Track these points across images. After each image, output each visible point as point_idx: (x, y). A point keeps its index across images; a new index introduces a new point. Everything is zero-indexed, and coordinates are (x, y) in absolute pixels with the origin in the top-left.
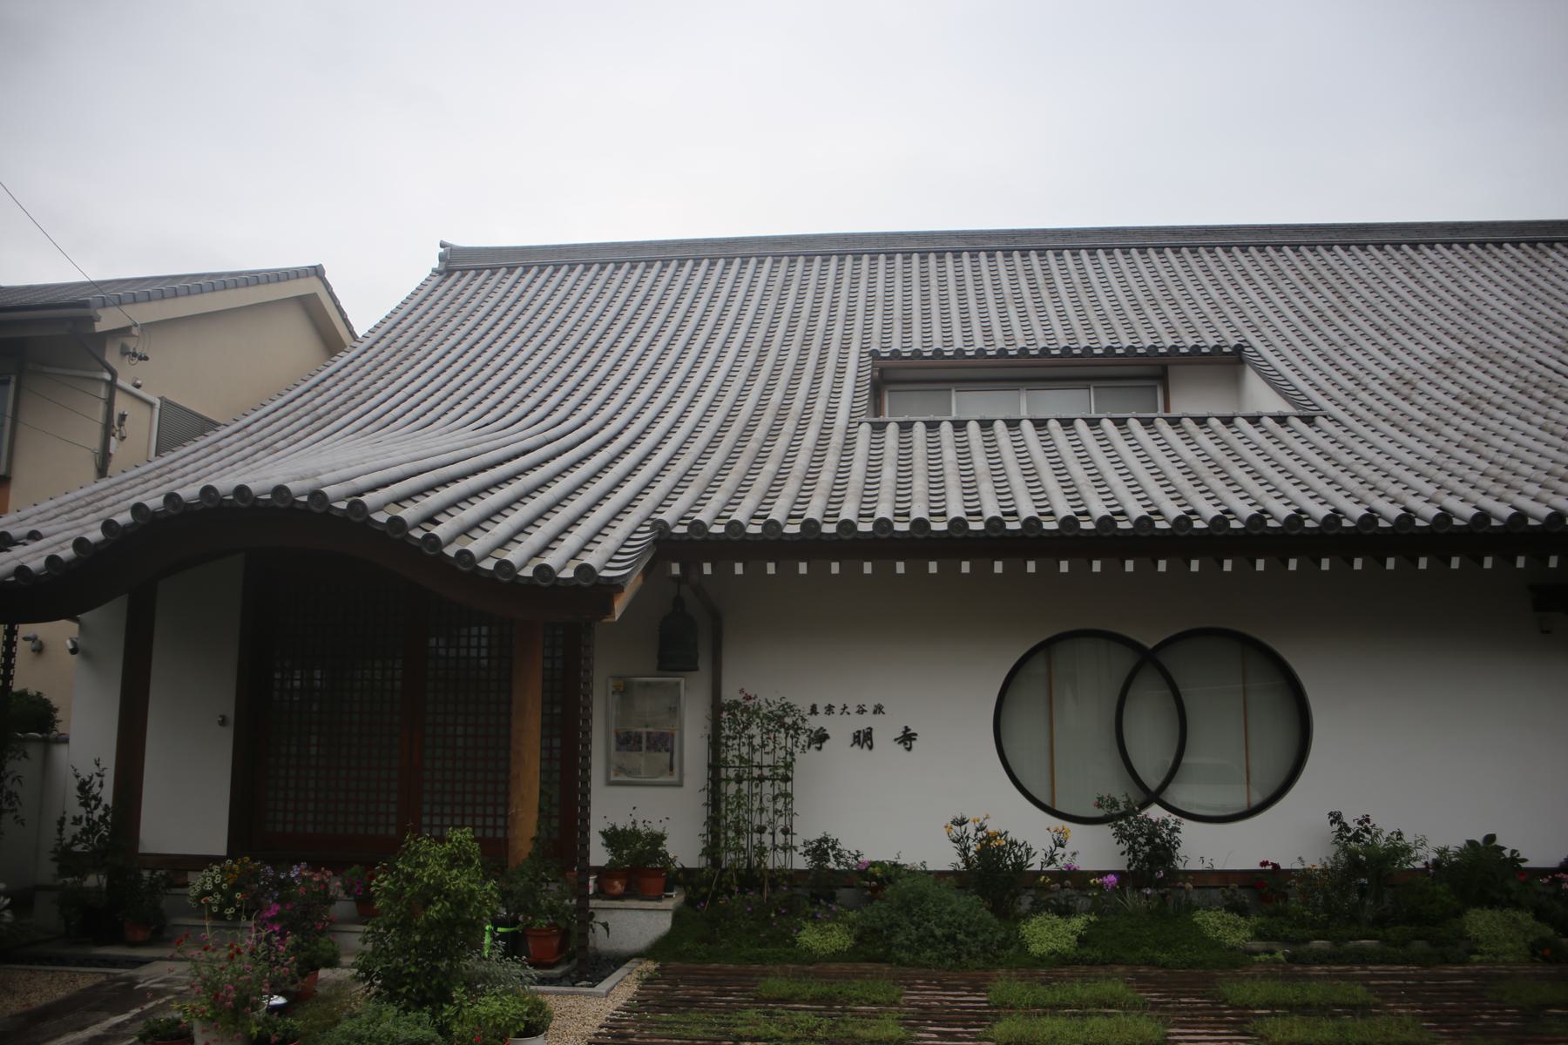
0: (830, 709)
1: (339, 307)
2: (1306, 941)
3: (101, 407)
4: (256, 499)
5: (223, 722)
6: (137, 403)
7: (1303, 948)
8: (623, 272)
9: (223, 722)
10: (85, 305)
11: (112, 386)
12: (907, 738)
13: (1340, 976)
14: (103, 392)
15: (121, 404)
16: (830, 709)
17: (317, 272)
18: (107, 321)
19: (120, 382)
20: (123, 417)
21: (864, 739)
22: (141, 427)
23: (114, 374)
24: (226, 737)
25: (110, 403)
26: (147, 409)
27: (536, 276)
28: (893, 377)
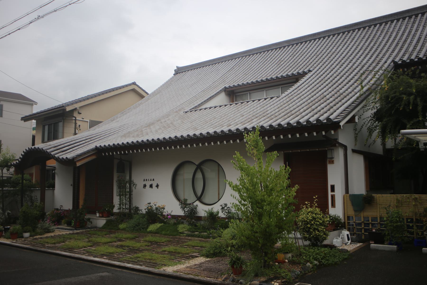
0: (146, 180)
1: (144, 91)
2: (194, 232)
3: (74, 124)
4: (226, 133)
5: (71, 185)
6: (84, 122)
7: (193, 234)
8: (382, 26)
9: (71, 185)
10: (63, 106)
11: (76, 120)
12: (157, 186)
13: (200, 241)
14: (74, 121)
15: (78, 123)
16: (146, 180)
17: (134, 83)
18: (68, 109)
19: (77, 119)
20: (79, 126)
21: (151, 186)
22: (85, 126)
23: (75, 118)
24: (72, 187)
25: (76, 124)
26: (87, 123)
27: (352, 33)
28: (234, 94)
